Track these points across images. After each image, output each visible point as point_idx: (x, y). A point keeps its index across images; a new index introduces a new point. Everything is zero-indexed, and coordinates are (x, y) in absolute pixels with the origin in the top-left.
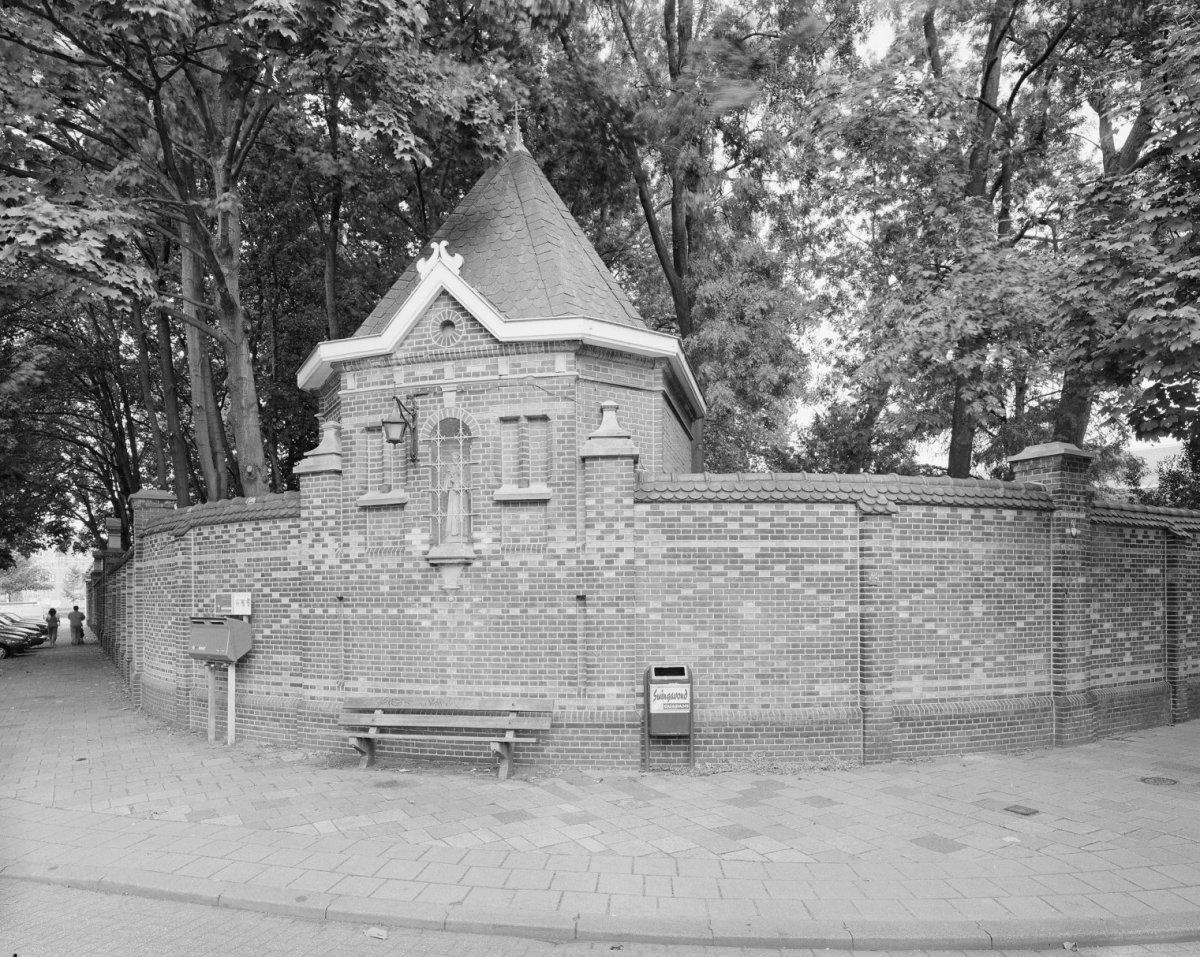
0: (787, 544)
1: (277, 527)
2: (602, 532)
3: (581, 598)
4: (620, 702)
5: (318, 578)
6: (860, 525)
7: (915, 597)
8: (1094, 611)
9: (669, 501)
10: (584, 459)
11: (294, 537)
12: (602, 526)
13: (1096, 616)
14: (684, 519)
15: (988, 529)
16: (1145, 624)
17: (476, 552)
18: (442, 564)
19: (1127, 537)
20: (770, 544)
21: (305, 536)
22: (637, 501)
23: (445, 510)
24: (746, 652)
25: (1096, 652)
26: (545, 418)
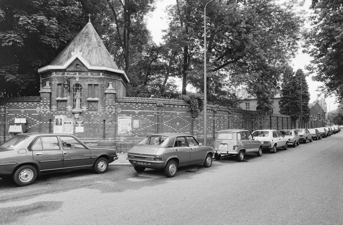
0: (144, 111)
1: (14, 104)
2: (109, 107)
3: (104, 120)
4: (112, 141)
5: (45, 115)
6: (157, 108)
7: (167, 121)
8: (199, 125)
9: (122, 102)
10: (105, 93)
11: (38, 106)
12: (109, 106)
13: (200, 126)
14: (125, 106)
15: (180, 109)
16: (209, 127)
17: (82, 111)
18: (75, 113)
19: (208, 111)
20: (141, 111)
21: (42, 106)
22: (116, 102)
23: (76, 102)
24: (136, 131)
25: (199, 132)
26: (97, 85)
